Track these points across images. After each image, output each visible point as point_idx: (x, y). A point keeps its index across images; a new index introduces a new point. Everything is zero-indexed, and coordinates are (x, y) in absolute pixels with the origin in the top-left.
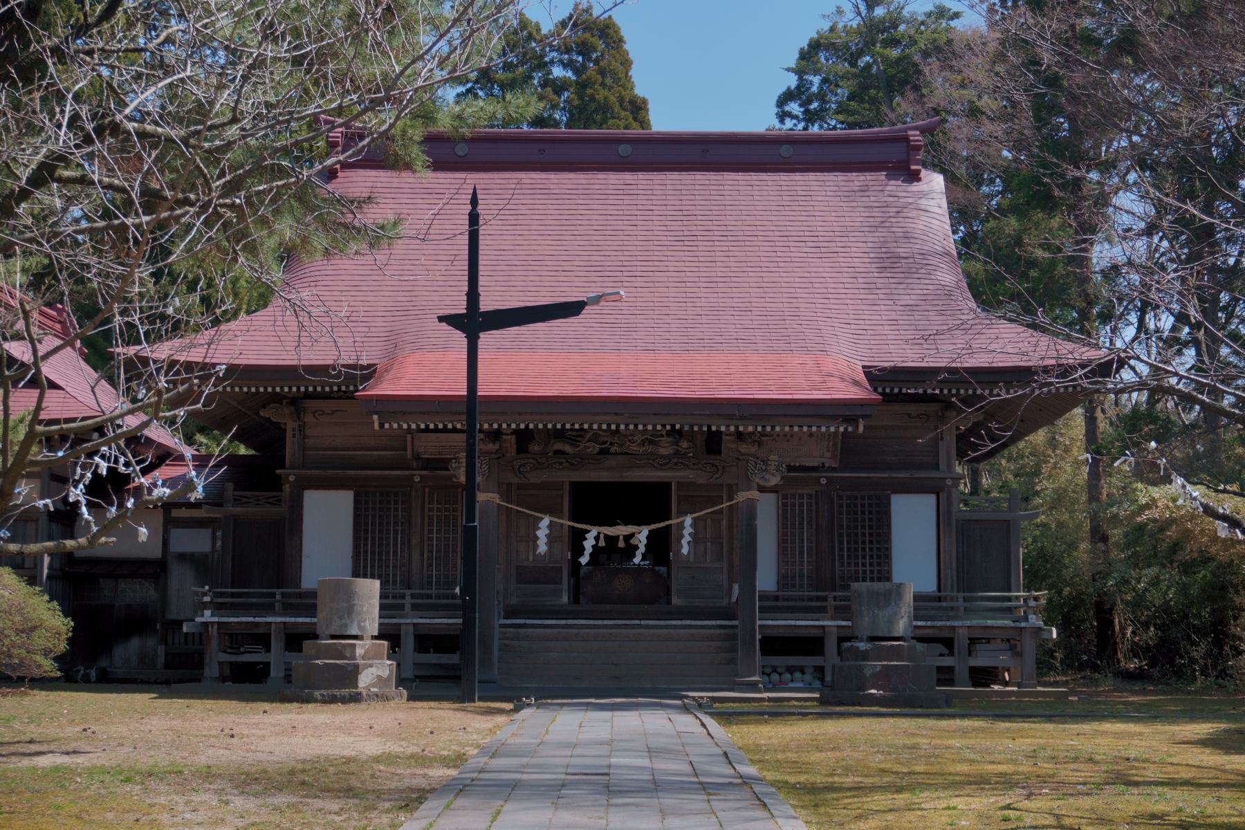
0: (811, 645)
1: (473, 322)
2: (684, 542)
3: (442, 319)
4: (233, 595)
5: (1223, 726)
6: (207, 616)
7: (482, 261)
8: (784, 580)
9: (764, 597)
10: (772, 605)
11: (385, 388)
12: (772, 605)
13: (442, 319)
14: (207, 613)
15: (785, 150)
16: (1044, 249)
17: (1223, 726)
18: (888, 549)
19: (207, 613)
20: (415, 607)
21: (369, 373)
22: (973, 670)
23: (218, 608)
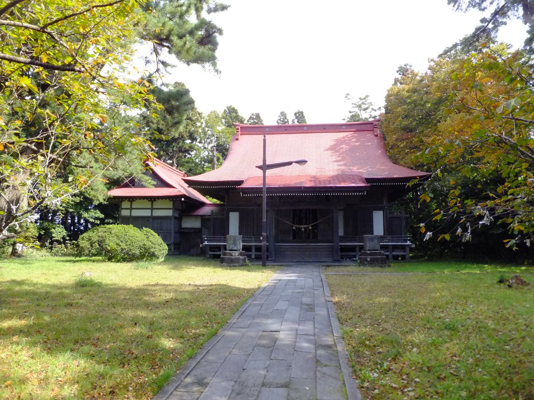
0: (352, 249)
1: (264, 167)
2: (306, 328)
3: (256, 167)
4: (213, 238)
5: (240, 187)
6: (206, 243)
7: (267, 154)
8: (345, 232)
9: (341, 237)
10: (342, 239)
11: (243, 186)
12: (342, 239)
13: (256, 167)
14: (206, 242)
15: (344, 127)
16: (524, 62)
17: (240, 187)
18: (373, 226)
19: (206, 242)
20: (255, 240)
21: (241, 182)
22: (394, 256)
23: (208, 241)
